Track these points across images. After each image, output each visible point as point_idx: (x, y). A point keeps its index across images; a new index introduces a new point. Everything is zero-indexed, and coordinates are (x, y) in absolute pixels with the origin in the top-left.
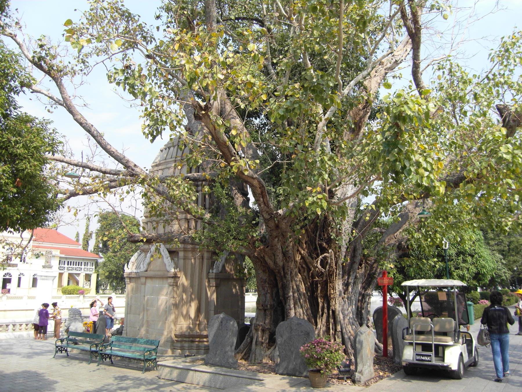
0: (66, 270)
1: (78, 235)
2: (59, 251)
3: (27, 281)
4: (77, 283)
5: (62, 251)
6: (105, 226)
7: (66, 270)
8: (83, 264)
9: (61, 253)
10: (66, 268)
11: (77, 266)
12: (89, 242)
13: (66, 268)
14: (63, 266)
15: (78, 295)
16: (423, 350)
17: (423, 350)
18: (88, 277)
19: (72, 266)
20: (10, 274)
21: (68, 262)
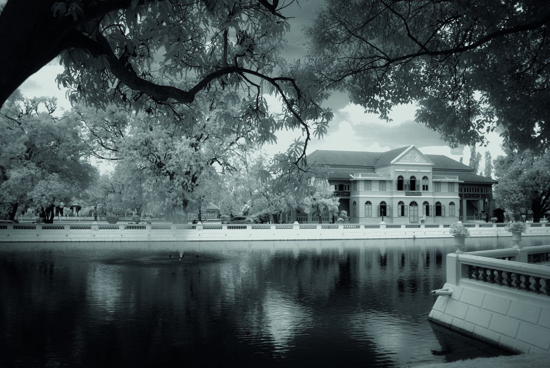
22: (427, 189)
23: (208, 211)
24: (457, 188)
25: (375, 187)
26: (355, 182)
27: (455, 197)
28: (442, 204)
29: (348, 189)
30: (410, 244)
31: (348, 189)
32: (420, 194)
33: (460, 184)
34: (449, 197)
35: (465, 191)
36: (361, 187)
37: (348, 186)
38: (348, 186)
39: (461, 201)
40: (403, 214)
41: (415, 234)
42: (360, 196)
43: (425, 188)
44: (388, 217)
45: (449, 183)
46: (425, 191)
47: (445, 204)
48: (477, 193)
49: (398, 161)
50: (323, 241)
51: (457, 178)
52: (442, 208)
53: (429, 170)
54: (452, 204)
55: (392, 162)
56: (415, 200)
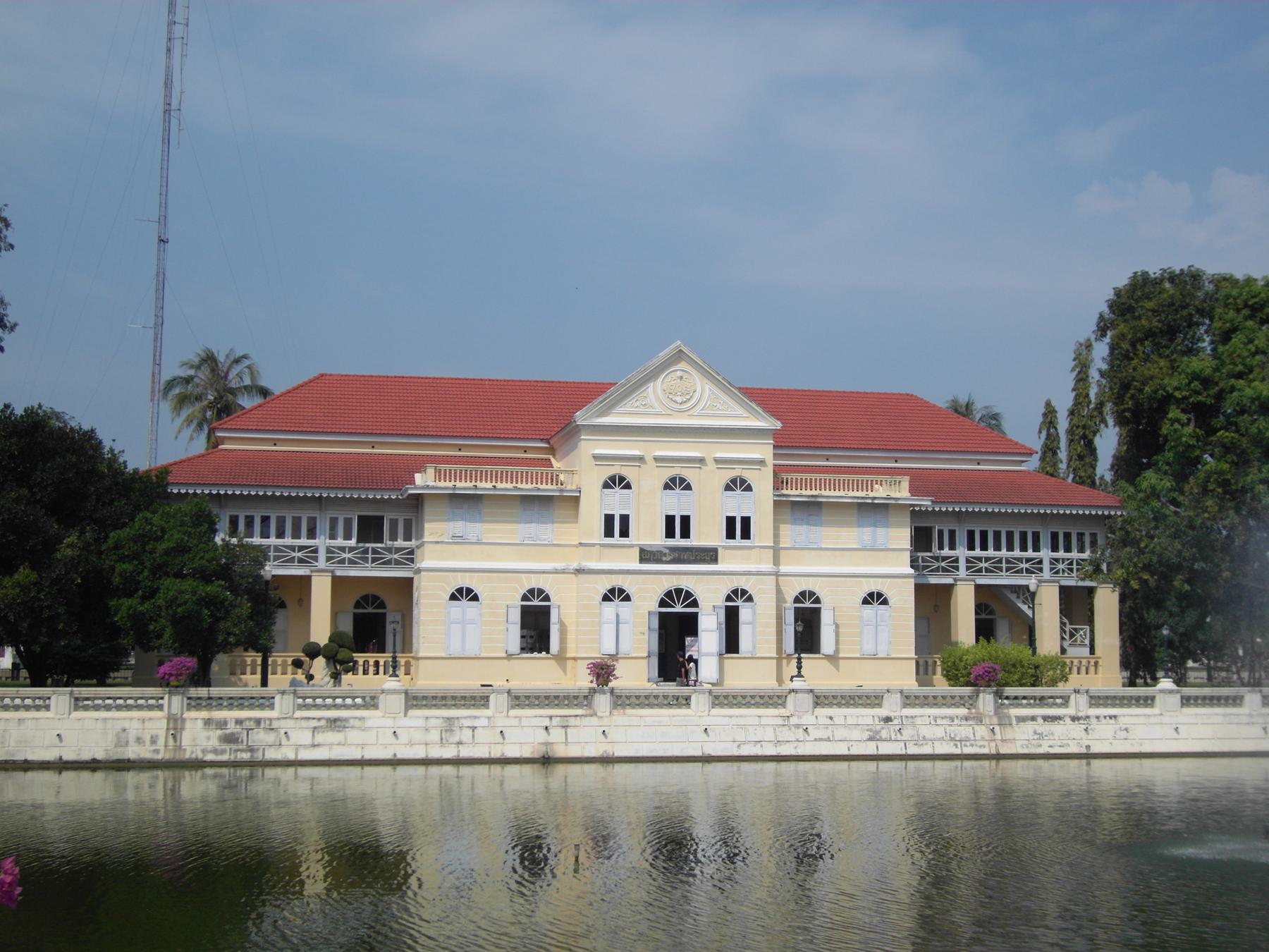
0: (962, 572)
1: (1049, 415)
2: (905, 483)
3: (762, 627)
4: (1029, 632)
5: (919, 484)
6: (1125, 346)
7: (962, 572)
8: (1045, 540)
9: (914, 490)
10: (962, 564)
11: (1017, 553)
12: (1098, 441)
13: (962, 564)
14: (946, 552)
15: (967, 690)
16: (642, 560)
17: (642, 560)
18: (1076, 606)
19: (991, 552)
20: (689, 595)
21: (971, 535)
32: (710, 555)
33: (916, 514)
36: (435, 529)
43: (738, 528)
52: (826, 619)
56: (686, 583)
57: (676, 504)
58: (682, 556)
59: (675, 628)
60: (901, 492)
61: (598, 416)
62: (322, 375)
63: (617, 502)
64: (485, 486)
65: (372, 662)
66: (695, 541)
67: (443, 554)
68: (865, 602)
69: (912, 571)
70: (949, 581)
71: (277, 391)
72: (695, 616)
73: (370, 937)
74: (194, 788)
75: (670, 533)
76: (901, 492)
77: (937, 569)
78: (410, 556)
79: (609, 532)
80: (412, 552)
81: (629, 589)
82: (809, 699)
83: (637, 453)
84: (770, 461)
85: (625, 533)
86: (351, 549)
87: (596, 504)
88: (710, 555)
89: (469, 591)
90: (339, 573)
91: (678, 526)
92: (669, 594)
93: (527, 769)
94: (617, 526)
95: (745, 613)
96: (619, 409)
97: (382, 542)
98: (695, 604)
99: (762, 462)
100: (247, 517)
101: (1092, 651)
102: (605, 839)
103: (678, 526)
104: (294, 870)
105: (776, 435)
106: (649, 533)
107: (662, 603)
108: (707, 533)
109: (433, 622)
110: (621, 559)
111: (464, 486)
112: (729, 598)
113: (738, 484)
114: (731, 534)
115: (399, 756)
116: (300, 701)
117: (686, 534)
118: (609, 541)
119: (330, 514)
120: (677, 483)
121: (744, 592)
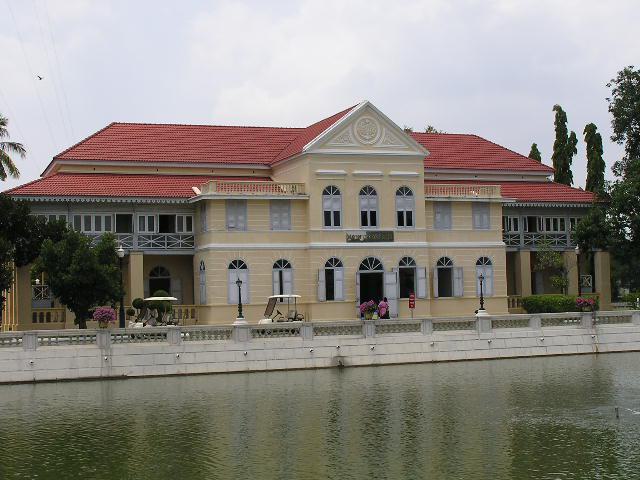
20: (377, 261)
22: (410, 223)
23: (281, 273)
24: (496, 217)
25: (259, 219)
26: (203, 205)
27: (493, 243)
28: (456, 263)
29: (189, 228)
30: (90, 397)
31: (189, 228)
32: (388, 236)
33: (506, 209)
34: (476, 242)
35: (548, 229)
36: (215, 219)
37: (189, 220)
38: (189, 220)
39: (512, 259)
40: (330, 295)
41: (344, 352)
42: (212, 245)
43: (405, 219)
44: (460, 298)
45: (477, 205)
46: (405, 228)
47: (464, 264)
48: (559, 232)
49: (323, 144)
50: (252, 375)
51: (498, 190)
52: (456, 274)
53: (417, 171)
54: (483, 261)
55: (307, 147)
56: (376, 255)
57: (367, 204)
58: (373, 237)
59: (370, 286)
60: (496, 195)
61: (320, 148)
62: (114, 123)
63: (331, 205)
64: (247, 195)
65: (190, 310)
66: (381, 227)
67: (218, 243)
68: (231, 267)
69: (504, 244)
70: (515, 250)
71: (542, 162)
72: (381, 275)
73: (592, 424)
74: (121, 391)
75: (364, 223)
76: (496, 195)
77: (149, 245)
78: (191, 241)
79: (328, 223)
80: (193, 238)
81: (247, 262)
82: (488, 324)
83: (342, 171)
84: (423, 177)
85: (337, 223)
86: (154, 237)
87: (318, 205)
88: (388, 236)
89: (241, 262)
90: (148, 253)
91: (369, 218)
92: (365, 261)
93: (328, 371)
94: (332, 219)
95: (338, 274)
96: (331, 143)
97: (174, 232)
98: (380, 267)
99: (417, 177)
100: (85, 217)
101: (594, 290)
102: (415, 405)
103: (369, 218)
104: (554, 395)
105: (426, 160)
106: (352, 224)
107: (362, 268)
108: (387, 223)
109: (216, 285)
110: (332, 242)
111: (235, 195)
112: (327, 265)
113: (404, 191)
114: (401, 223)
115: (37, 379)
116: (40, 339)
117: (374, 223)
118: (328, 228)
119: (75, 213)
120: (368, 191)
121: (336, 260)
